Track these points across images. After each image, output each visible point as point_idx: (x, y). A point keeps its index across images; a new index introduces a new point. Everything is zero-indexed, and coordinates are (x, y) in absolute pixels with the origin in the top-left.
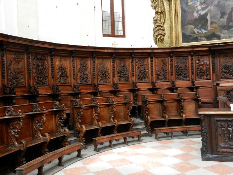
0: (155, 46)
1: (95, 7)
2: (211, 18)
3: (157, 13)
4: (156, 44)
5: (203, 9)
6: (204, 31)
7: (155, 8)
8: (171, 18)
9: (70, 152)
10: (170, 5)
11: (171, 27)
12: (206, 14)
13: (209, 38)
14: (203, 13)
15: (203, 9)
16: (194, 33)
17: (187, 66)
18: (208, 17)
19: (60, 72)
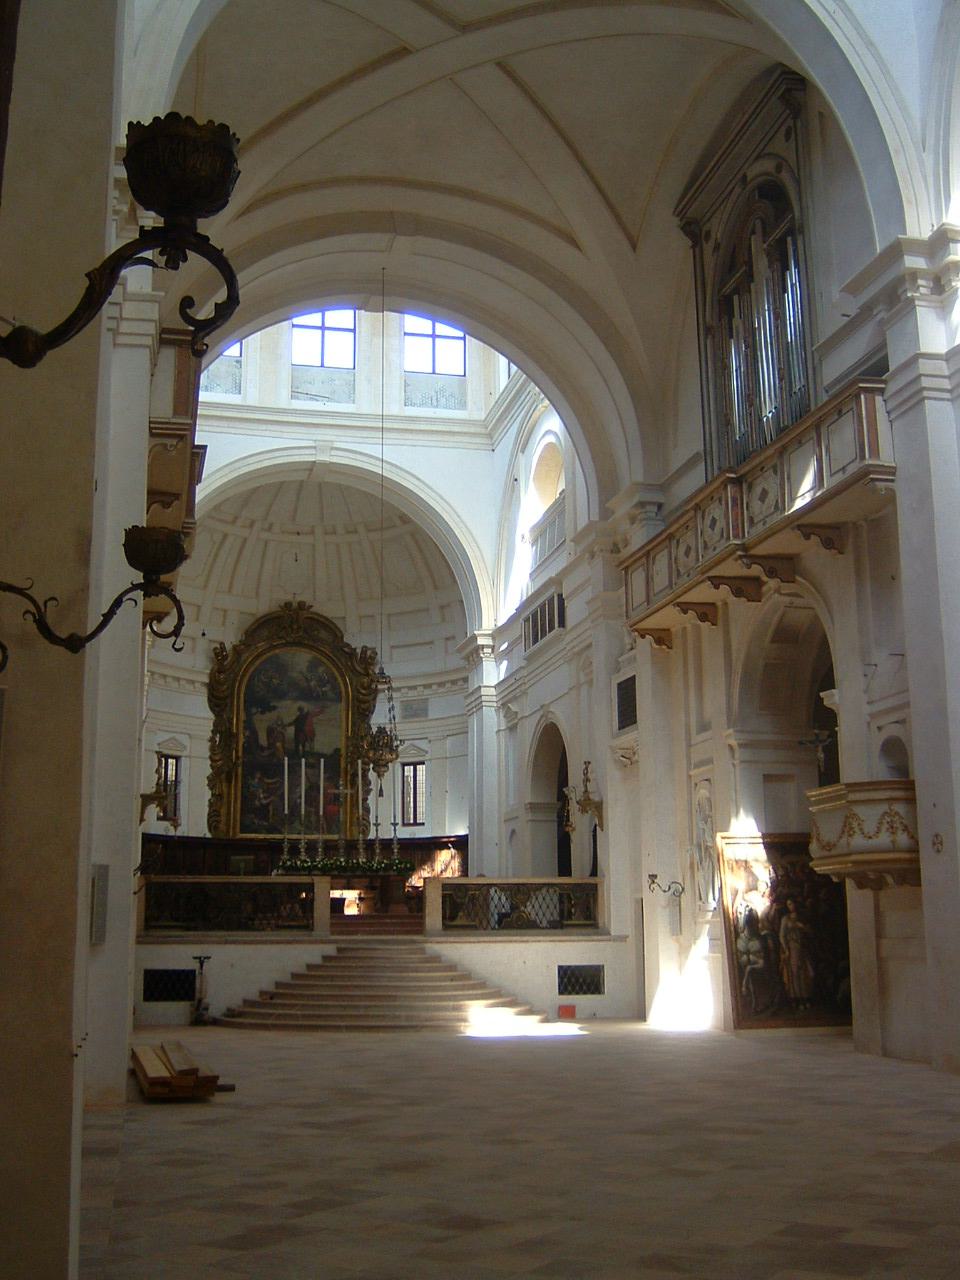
0: (209, 835)
1: (298, 534)
2: (274, 810)
3: (213, 795)
4: (210, 830)
5: (265, 798)
6: (265, 823)
7: (211, 789)
8: (229, 803)
9: (155, 378)
10: (229, 787)
11: (229, 813)
12: (268, 804)
13: (269, 831)
14: (264, 802)
15: (265, 798)
16: (254, 823)
17: (566, 922)
18: (271, 808)
19: (292, 629)
